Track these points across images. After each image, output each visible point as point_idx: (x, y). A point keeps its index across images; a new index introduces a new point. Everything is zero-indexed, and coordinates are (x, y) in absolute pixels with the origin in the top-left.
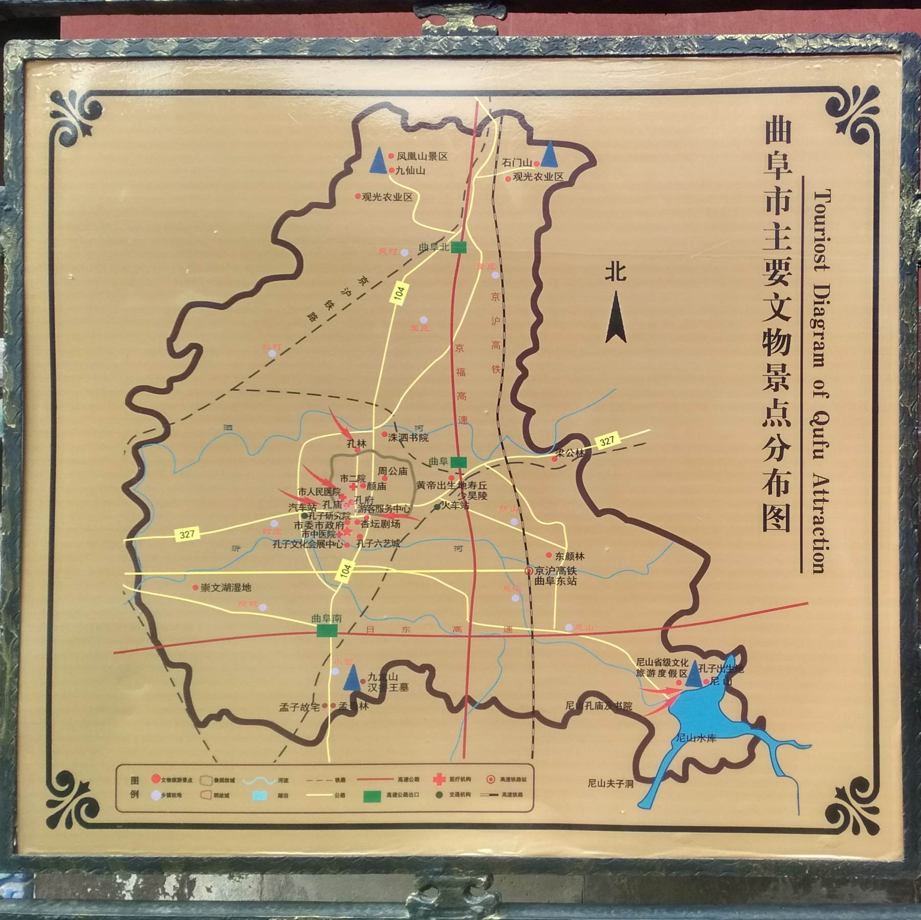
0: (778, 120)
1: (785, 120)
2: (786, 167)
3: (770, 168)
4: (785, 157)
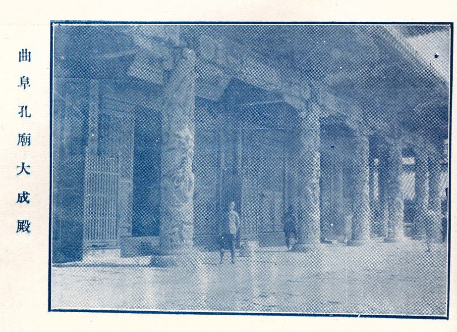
0: (25, 51)
1: (28, 52)
2: (28, 83)
3: (22, 84)
4: (28, 79)
